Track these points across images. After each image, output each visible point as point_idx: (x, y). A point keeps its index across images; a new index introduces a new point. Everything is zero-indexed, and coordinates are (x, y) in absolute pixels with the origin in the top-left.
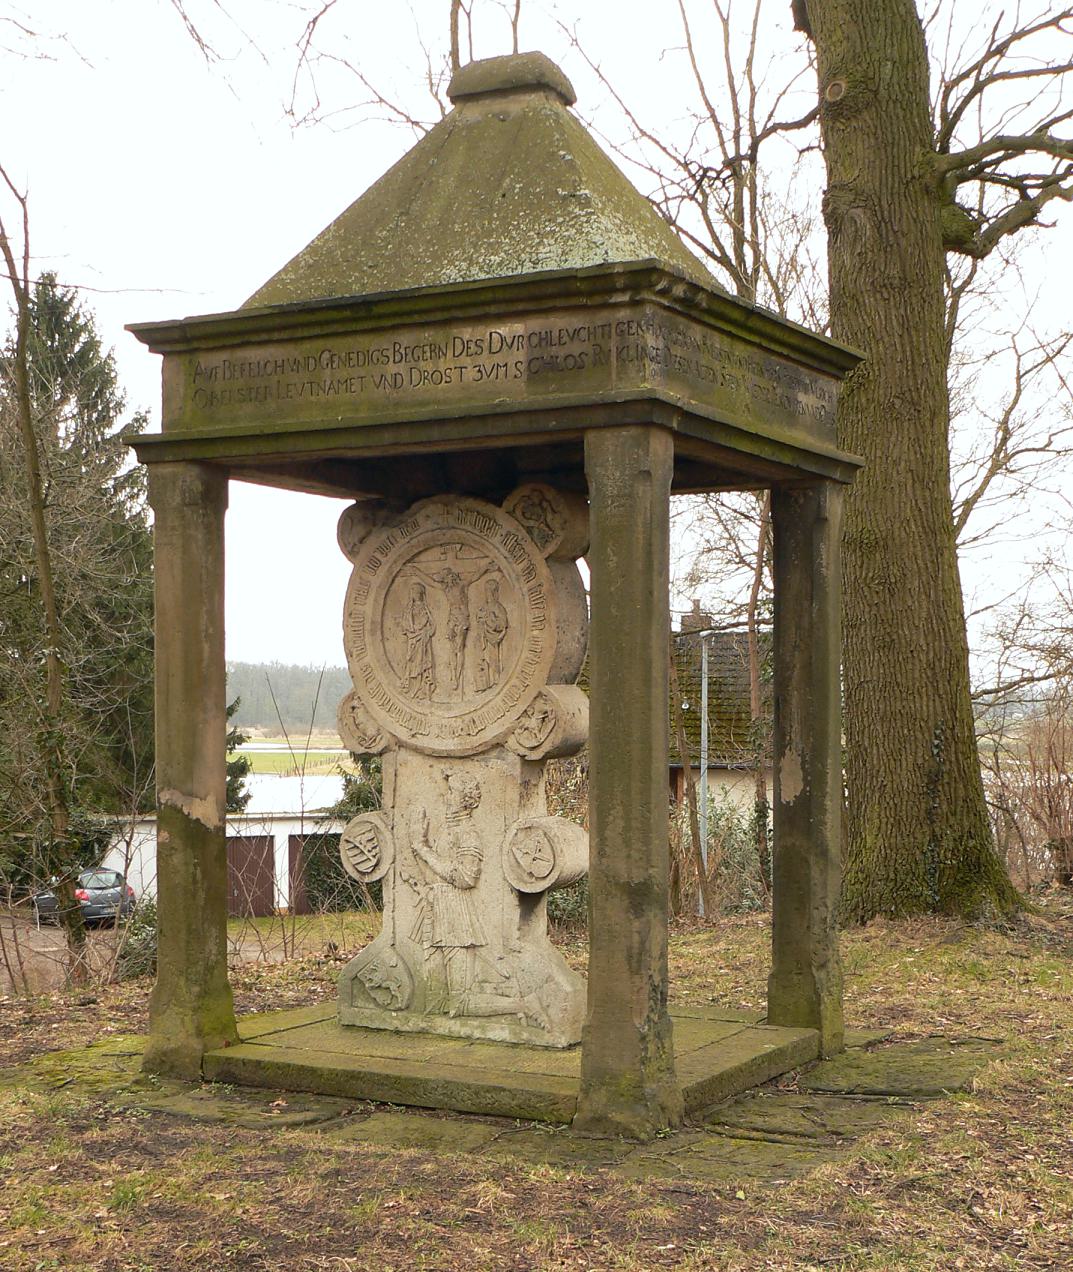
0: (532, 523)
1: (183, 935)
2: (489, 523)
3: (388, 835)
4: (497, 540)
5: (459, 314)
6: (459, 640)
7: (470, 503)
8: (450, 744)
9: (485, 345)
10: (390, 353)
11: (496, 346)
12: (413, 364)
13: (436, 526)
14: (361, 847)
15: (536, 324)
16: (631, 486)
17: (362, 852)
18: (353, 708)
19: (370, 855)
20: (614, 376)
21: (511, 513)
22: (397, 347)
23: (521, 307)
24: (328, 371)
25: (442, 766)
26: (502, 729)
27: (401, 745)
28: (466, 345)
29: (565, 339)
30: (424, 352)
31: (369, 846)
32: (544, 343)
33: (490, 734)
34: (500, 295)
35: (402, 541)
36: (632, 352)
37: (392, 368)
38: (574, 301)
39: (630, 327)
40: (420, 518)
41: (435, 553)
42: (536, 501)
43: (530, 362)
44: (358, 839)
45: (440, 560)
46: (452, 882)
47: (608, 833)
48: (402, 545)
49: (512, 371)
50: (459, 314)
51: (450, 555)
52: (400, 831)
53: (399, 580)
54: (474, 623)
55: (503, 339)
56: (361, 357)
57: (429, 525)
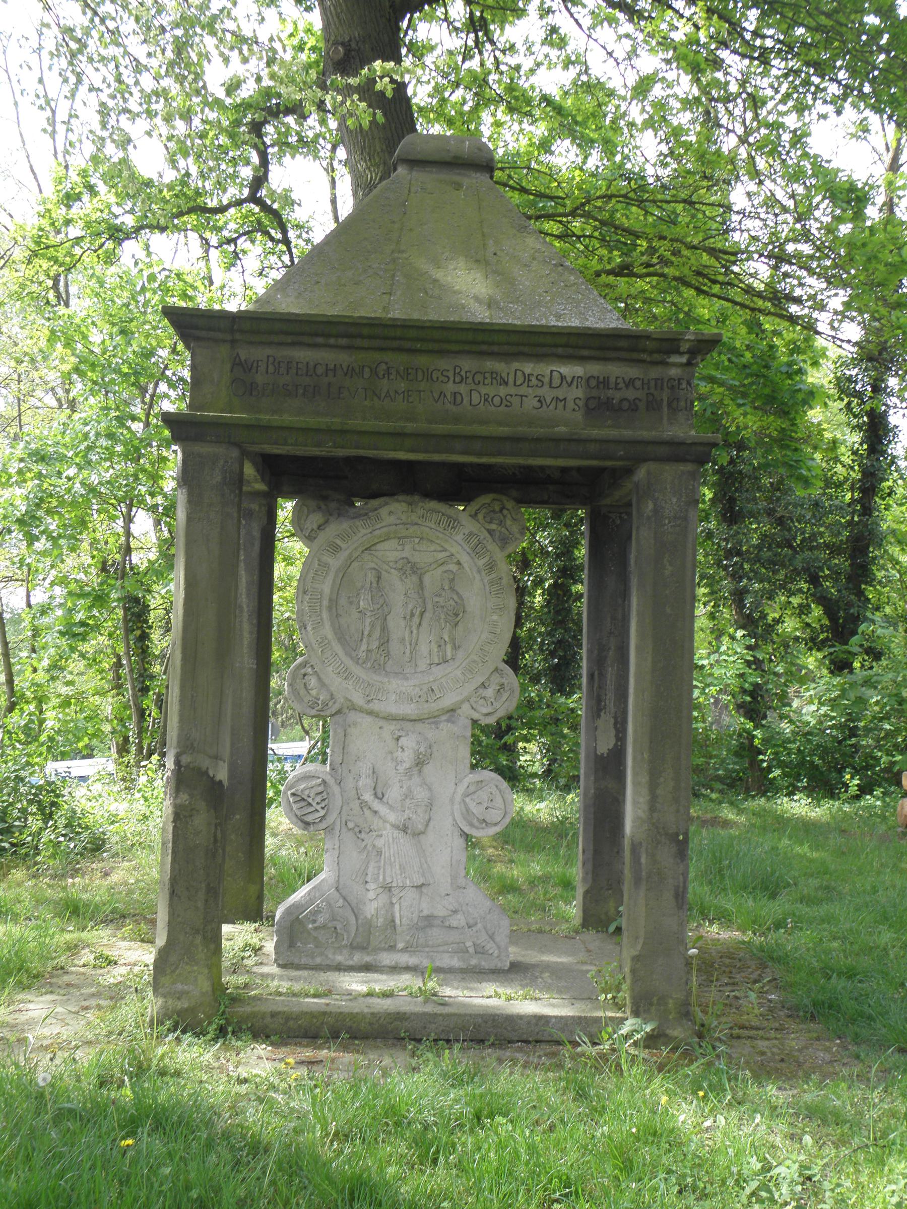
0: (493, 526)
1: (201, 895)
2: (453, 523)
3: (336, 789)
4: (459, 538)
5: (526, 349)
6: (416, 620)
7: (433, 504)
8: (409, 709)
9: (546, 380)
10: (451, 374)
11: (556, 381)
12: (473, 386)
13: (398, 522)
14: (310, 800)
15: (595, 369)
16: (687, 511)
17: (310, 804)
18: (305, 675)
19: (318, 807)
20: (665, 418)
21: (474, 516)
22: (458, 370)
23: (585, 353)
24: (385, 381)
25: (392, 728)
26: (459, 698)
27: (353, 708)
28: (527, 378)
29: (622, 385)
30: (485, 378)
31: (318, 799)
32: (601, 386)
33: (448, 701)
34: (365, 331)
35: (363, 531)
36: (682, 404)
37: (450, 387)
38: (635, 356)
39: (679, 384)
40: (384, 512)
41: (393, 543)
42: (497, 508)
43: (588, 399)
44: (307, 792)
45: (396, 550)
46: (404, 829)
47: (659, 792)
48: (363, 532)
49: (570, 405)
50: (526, 349)
51: (408, 547)
52: (349, 783)
53: (355, 565)
54: (430, 606)
55: (563, 378)
56: (420, 374)
57: (392, 519)
